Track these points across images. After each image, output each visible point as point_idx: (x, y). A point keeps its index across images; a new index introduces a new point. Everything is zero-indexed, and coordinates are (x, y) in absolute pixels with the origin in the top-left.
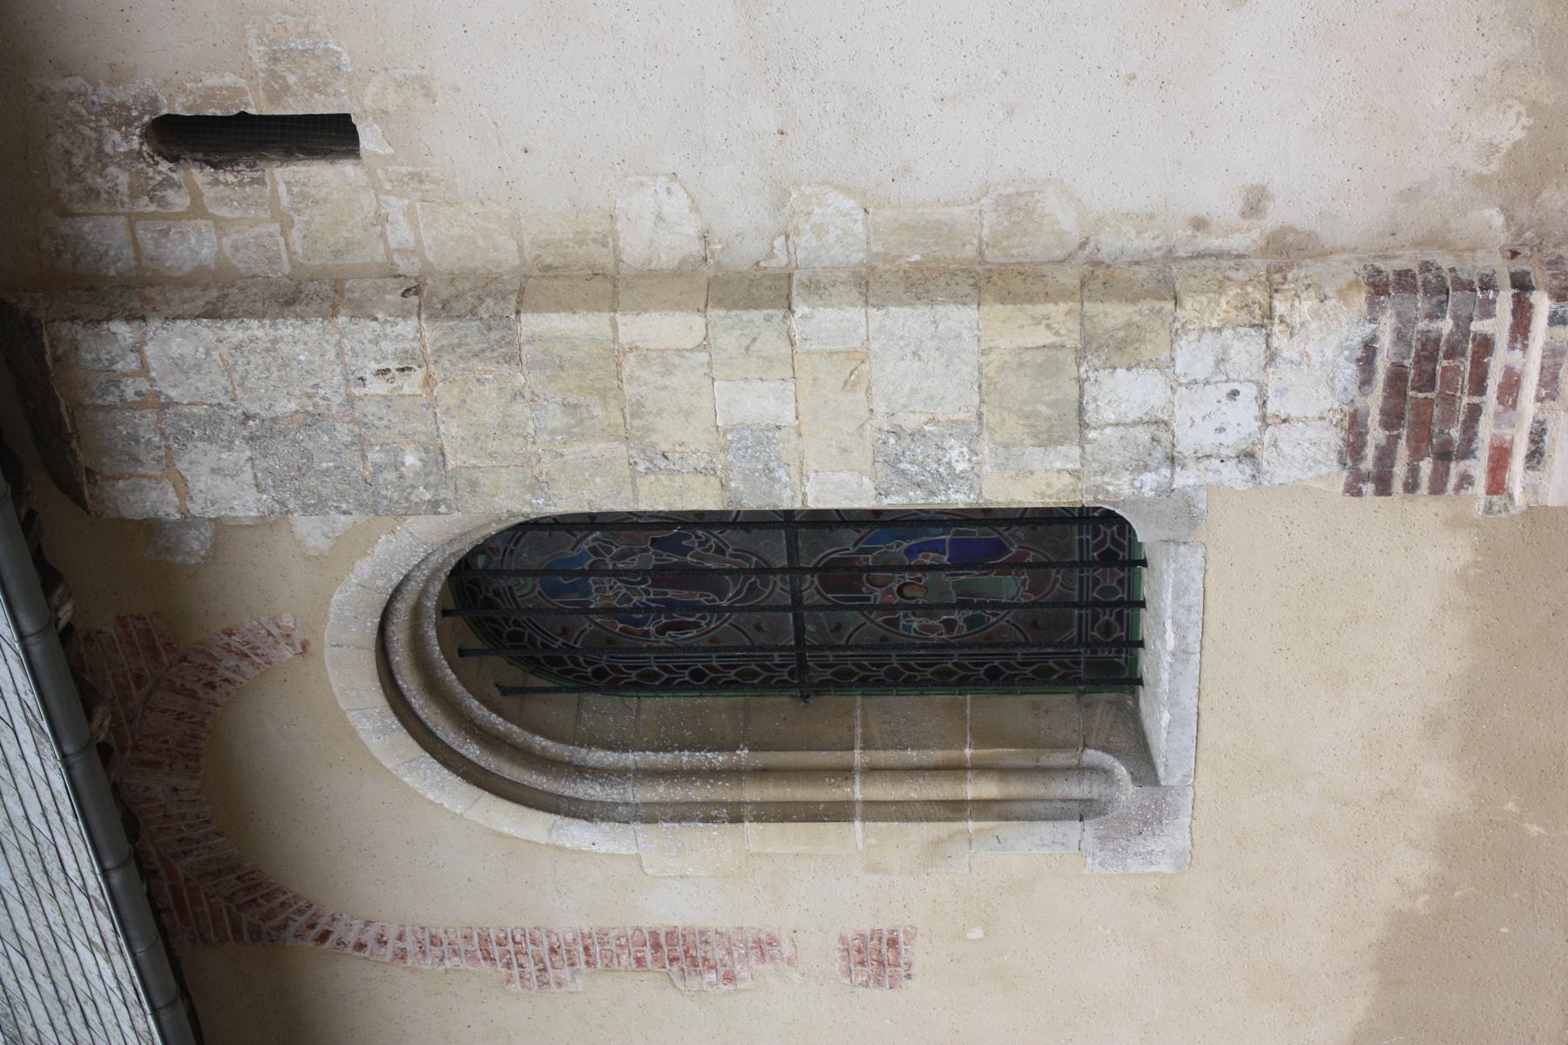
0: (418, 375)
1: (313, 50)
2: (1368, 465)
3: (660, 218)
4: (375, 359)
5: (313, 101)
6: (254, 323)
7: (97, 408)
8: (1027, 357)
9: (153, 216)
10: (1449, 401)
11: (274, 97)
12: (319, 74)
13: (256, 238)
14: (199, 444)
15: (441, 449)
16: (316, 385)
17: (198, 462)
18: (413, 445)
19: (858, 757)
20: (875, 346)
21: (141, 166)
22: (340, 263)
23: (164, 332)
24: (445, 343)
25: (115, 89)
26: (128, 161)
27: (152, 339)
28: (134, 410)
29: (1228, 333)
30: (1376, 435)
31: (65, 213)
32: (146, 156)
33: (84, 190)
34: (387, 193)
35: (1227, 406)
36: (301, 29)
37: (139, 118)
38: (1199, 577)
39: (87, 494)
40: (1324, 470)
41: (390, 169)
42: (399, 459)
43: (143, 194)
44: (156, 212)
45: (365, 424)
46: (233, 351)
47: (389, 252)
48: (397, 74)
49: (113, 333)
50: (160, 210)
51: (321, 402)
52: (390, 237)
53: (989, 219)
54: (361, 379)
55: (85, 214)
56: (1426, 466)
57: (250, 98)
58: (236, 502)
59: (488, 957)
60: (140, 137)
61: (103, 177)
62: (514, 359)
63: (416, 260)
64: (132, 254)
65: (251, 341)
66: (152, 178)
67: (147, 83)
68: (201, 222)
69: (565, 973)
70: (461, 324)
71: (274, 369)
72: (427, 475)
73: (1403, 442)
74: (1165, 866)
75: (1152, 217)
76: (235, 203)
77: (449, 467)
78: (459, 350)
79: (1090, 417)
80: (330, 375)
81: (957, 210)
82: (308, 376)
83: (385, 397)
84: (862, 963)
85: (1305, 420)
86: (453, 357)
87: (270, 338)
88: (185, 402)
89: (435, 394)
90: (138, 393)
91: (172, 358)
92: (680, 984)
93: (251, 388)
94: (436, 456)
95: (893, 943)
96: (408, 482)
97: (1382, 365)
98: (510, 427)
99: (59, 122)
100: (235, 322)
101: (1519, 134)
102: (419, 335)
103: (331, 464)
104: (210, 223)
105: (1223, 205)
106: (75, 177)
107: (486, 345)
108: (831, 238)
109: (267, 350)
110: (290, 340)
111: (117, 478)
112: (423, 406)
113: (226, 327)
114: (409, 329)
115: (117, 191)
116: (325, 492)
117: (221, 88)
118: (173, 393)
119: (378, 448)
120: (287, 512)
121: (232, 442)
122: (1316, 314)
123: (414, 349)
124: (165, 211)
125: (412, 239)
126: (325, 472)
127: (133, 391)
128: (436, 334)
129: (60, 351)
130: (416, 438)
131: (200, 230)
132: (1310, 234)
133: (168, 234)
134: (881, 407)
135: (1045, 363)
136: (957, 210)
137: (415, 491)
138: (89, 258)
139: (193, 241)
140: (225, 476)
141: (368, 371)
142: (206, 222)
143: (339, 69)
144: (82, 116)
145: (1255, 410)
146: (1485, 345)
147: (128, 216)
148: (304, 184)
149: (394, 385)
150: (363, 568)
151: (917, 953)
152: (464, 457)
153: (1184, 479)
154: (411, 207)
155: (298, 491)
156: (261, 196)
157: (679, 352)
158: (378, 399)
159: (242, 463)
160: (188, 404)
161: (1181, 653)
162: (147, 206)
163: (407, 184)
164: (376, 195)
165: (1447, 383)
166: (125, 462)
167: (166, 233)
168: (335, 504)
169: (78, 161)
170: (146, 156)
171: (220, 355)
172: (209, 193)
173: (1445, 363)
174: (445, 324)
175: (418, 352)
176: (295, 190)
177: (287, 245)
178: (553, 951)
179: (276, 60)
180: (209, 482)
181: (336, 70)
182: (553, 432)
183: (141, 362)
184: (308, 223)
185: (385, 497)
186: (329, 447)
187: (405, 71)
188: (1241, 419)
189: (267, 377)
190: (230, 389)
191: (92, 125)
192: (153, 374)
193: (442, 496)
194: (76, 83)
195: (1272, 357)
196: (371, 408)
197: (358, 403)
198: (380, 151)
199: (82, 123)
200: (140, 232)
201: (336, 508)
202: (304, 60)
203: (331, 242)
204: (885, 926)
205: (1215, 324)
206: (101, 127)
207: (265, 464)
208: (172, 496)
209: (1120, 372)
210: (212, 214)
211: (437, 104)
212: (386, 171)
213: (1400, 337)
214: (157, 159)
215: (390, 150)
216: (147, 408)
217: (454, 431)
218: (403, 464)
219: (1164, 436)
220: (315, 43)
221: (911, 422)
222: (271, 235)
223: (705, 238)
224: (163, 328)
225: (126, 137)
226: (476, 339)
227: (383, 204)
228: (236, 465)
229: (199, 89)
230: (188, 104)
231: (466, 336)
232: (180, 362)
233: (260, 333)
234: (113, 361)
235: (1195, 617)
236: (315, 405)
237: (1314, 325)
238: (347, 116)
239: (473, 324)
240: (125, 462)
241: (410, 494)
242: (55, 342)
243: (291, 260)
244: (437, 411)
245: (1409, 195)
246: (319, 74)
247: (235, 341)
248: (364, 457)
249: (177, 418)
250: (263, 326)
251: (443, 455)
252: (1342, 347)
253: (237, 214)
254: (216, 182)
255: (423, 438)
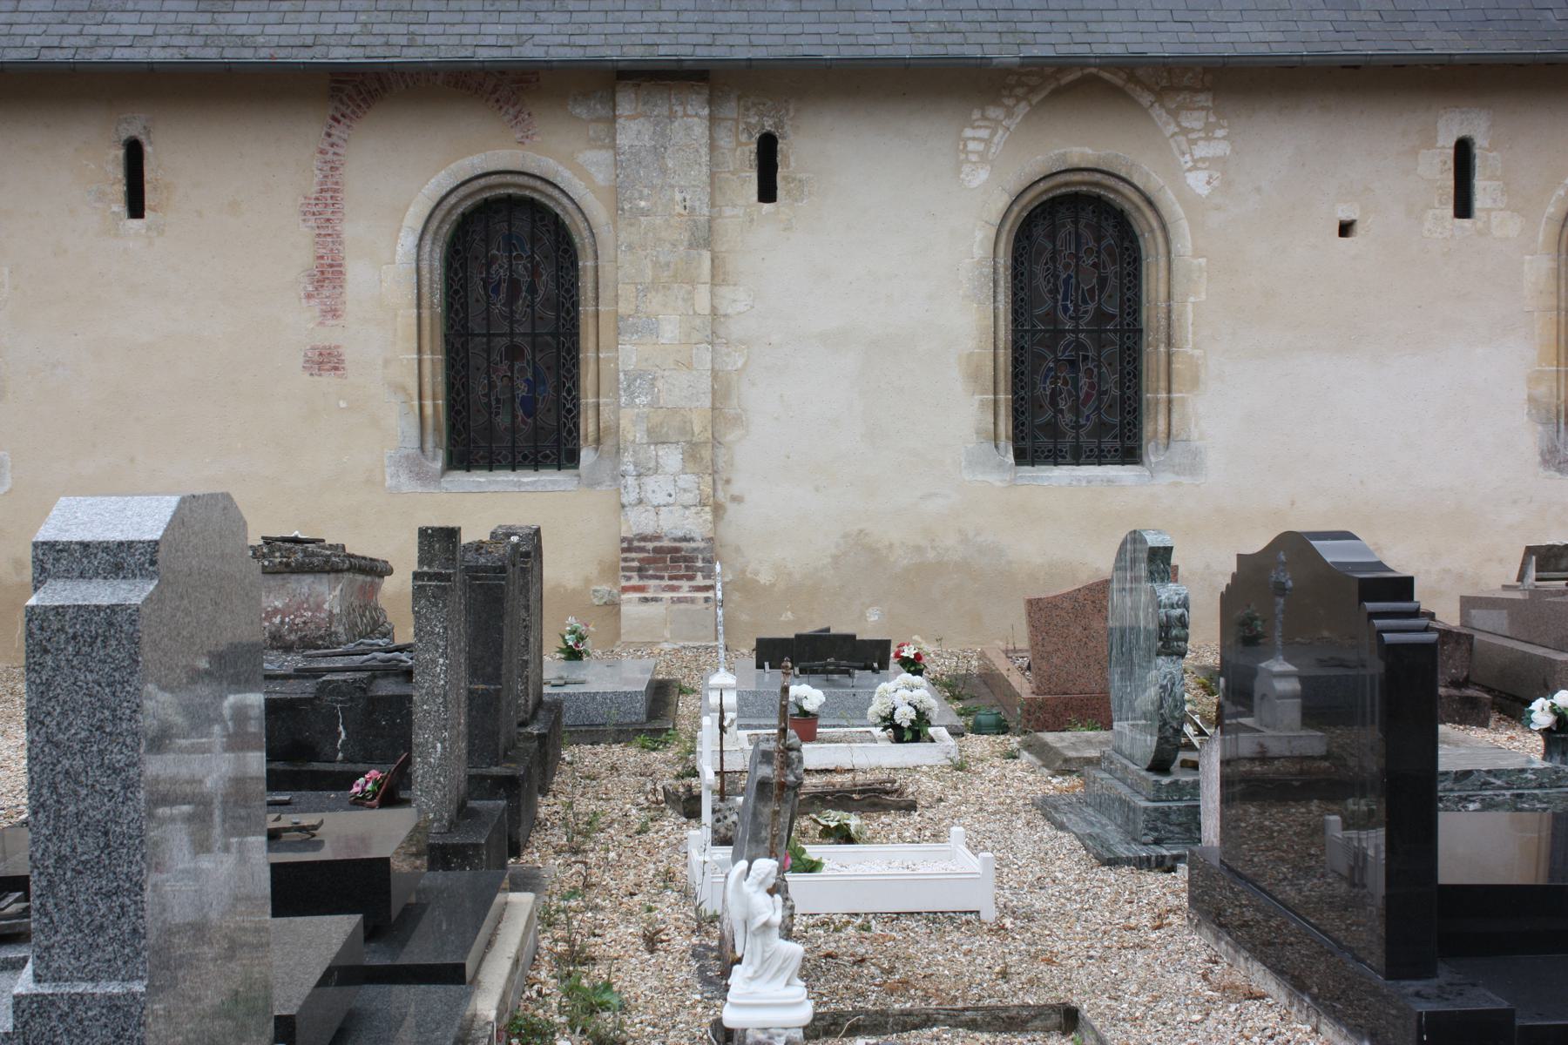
2: (636, 544)
3: (735, 301)
6: (708, 158)
7: (670, 95)
8: (688, 424)
9: (738, 128)
10: (666, 569)
11: (785, 178)
19: (1562, 369)
20: (694, 372)
29: (697, 492)
30: (650, 545)
35: (665, 493)
38: (562, 489)
40: (634, 529)
47: (720, 207)
53: (732, 411)
56: (636, 564)
59: (322, 191)
62: (691, 246)
69: (312, 223)
73: (646, 555)
74: (389, 482)
75: (732, 465)
79: (660, 446)
81: (736, 400)
84: (321, 354)
85: (658, 520)
92: (306, 273)
94: (645, 213)
95: (336, 369)
97: (684, 545)
101: (762, 582)
105: (735, 489)
106: (754, 105)
108: (725, 358)
116: (628, 170)
118: (676, 124)
122: (705, 521)
132: (722, 518)
134: (666, 373)
135: (685, 429)
136: (736, 400)
145: (662, 503)
146: (692, 578)
150: (567, 174)
151: (328, 380)
153: (630, 480)
157: (693, 305)
161: (520, 484)
165: (673, 568)
167: (730, 130)
169: (761, 107)
172: (746, 149)
173: (683, 566)
178: (328, 220)
182: (657, 257)
188: (660, 498)
194: (792, 114)
195: (686, 507)
204: (346, 365)
205: (702, 487)
208: (627, 113)
209: (681, 456)
213: (695, 550)
219: (651, 472)
221: (660, 384)
223: (725, 316)
225: (770, 126)
235: (540, 489)
237: (701, 520)
238: (775, 201)
245: (738, 549)
248: (645, 187)
252: (690, 530)
254: (751, 152)
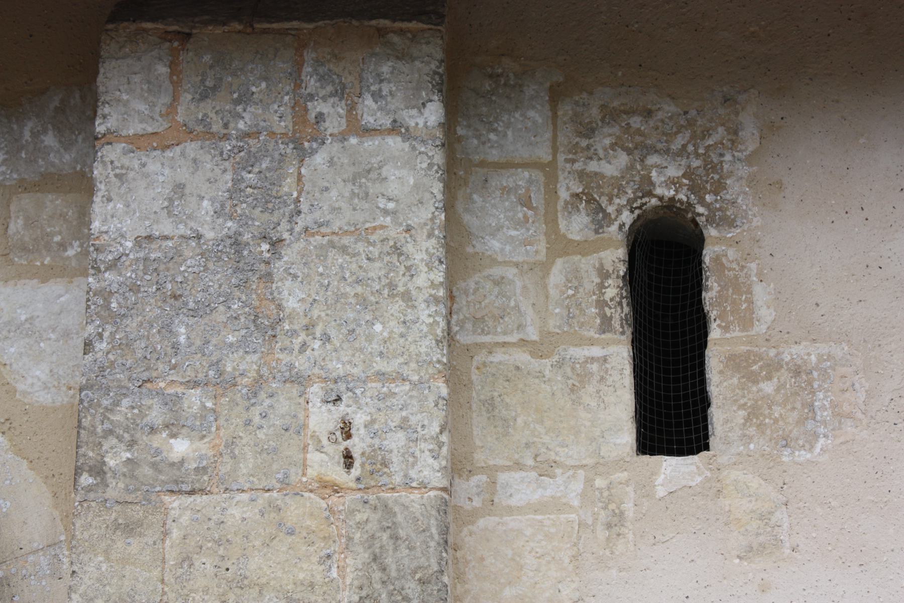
0: (337, 474)
1: (814, 419)
4: (373, 421)
5: (735, 408)
9: (551, 192)
12: (776, 421)
13: (517, 307)
14: (228, 176)
15: (202, 491)
16: (329, 339)
17: (197, 170)
18: (211, 453)
21: (630, 192)
22: (474, 406)
23: (425, 165)
24: (400, 518)
25: (744, 182)
26: (637, 178)
27: (414, 148)
28: (293, 108)
31: (556, 96)
32: (644, 200)
33: (591, 122)
34: (589, 482)
36: (846, 408)
37: (702, 202)
39: (148, 25)
41: (630, 489)
42: (184, 431)
43: (586, 187)
44: (558, 198)
45: (255, 395)
46: (391, 243)
48: (780, 515)
49: (424, 105)
50: (561, 204)
51: (298, 341)
52: (518, 475)
54: (339, 399)
55: (555, 116)
57: (736, 333)
58: (120, 206)
60: (672, 199)
61: (613, 146)
63: (477, 503)
64: (490, 159)
65: (408, 268)
66: (610, 201)
67: (755, 220)
68: (542, 246)
70: (432, 544)
71: (359, 289)
72: (154, 465)
76: (570, 292)
77: (167, 499)
78: (385, 536)
80: (346, 359)
82: (344, 331)
83: (305, 426)
86: (372, 527)
87: (413, 292)
88: (303, 171)
89: (307, 494)
90: (320, 117)
91: (380, 168)
93: (326, 257)
96: (143, 439)
98: (238, 591)
99: (693, 113)
100: (441, 253)
102: (414, 484)
103: (182, 339)
104: (542, 257)
107: (394, 574)
109: (392, 286)
110: (409, 317)
111: (173, 66)
112: (286, 476)
113: (433, 241)
114: (426, 473)
115: (591, 158)
116: (132, 324)
117: (750, 302)
119: (209, 404)
120: (99, 270)
121: (231, 218)
123: (390, 475)
124: (559, 208)
125: (514, 502)
126: (167, 329)
127: (325, 111)
128: (416, 508)
129: (396, 39)
130: (226, 458)
131: (531, 244)
133: (523, 205)
137: (123, 446)
138: (484, 109)
139: (513, 233)
140: (171, 200)
141: (349, 410)
142: (544, 251)
143: (785, 446)
144: (703, 138)
147: (553, 163)
148: (602, 379)
149: (325, 441)
152: (185, 519)
154: (566, 507)
155: (135, 289)
156: (582, 325)
158: (301, 416)
159: (192, 224)
160: (300, 173)
162: (568, 189)
163: (605, 508)
164: (583, 466)
166: (203, 81)
167: (526, 202)
168: (106, 334)
169: (636, 122)
170: (644, 200)
171: (382, 227)
172: (587, 264)
174: (433, 522)
175: (384, 480)
176: (595, 367)
177: (504, 344)
179: (797, 372)
180: (161, 179)
181: (784, 442)
183: (375, 130)
184: (540, 375)
185: (117, 403)
186: (214, 341)
187: (786, 526)
189: (345, 279)
190: (323, 230)
191: (690, 148)
192: (353, 141)
193: (112, 482)
194: (750, 138)
196: (283, 405)
197: (295, 390)
198: (660, 479)
199: (693, 137)
200: (526, 174)
201: (100, 335)
202: (798, 405)
203: (508, 400)
206: (688, 158)
207: (188, 253)
208: (135, 128)
210: (553, 263)
211: (737, 561)
212: (627, 483)
214: (637, 212)
215: (661, 492)
216: (295, 124)
217: (236, 513)
218: (174, 436)
220: (824, 423)
222: (520, 327)
224: (430, 165)
226: (406, 561)
227: (571, 472)
228: (190, 217)
229: (748, 276)
230: (724, 260)
231: (411, 548)
232: (373, 175)
233: (421, 280)
234: (377, 96)
236: (294, 333)
238: (707, 447)
239: (433, 561)
240: (203, 81)
241: (120, 438)
242: (409, 35)
243: (480, 346)
244: (275, 494)
246: (776, 421)
247: (410, 248)
249: (277, 156)
250: (433, 285)
251: (192, 492)
253: (553, 292)
254: (604, 275)
255: (224, 470)
